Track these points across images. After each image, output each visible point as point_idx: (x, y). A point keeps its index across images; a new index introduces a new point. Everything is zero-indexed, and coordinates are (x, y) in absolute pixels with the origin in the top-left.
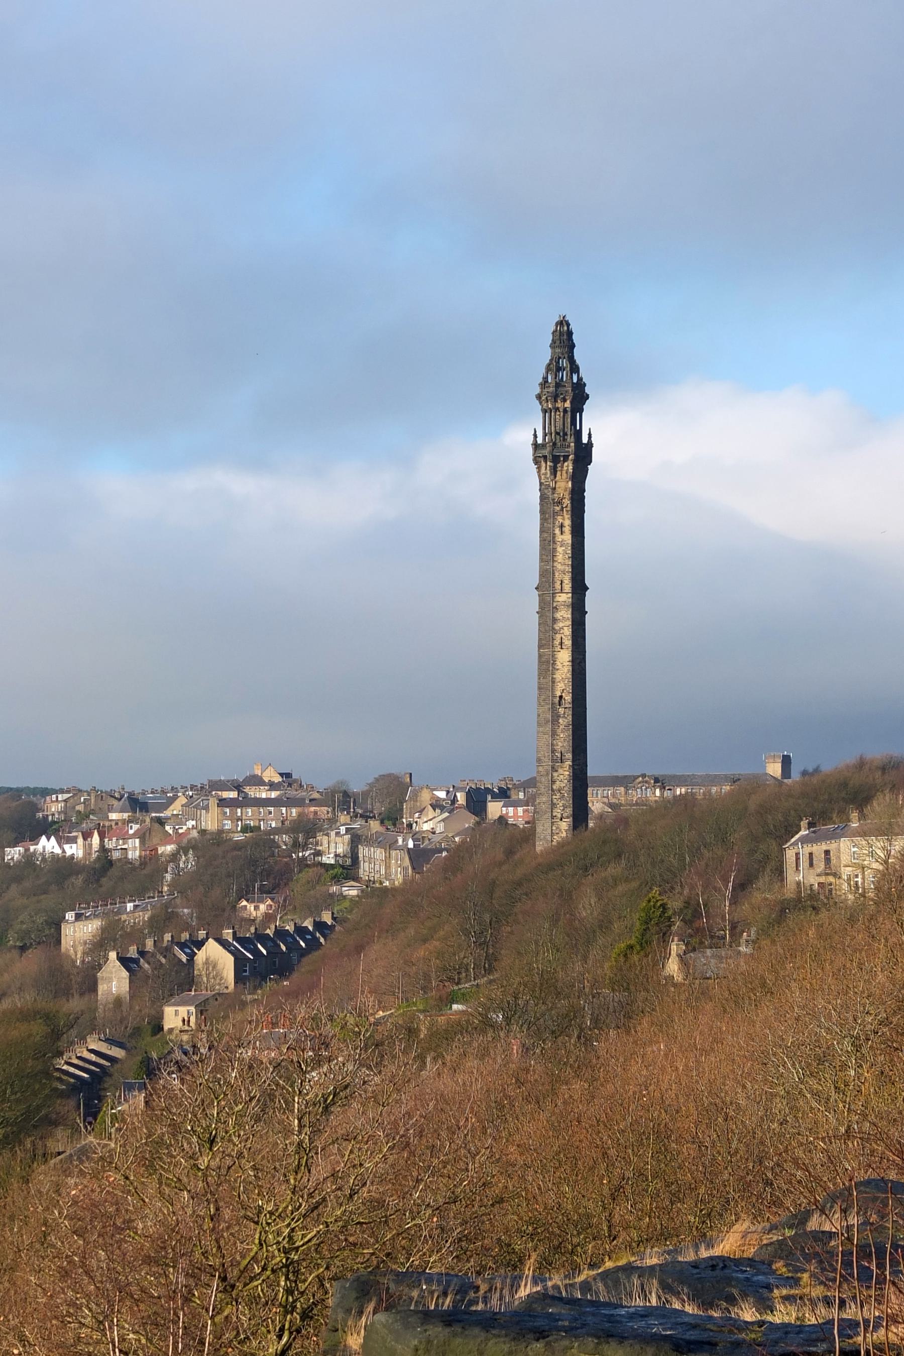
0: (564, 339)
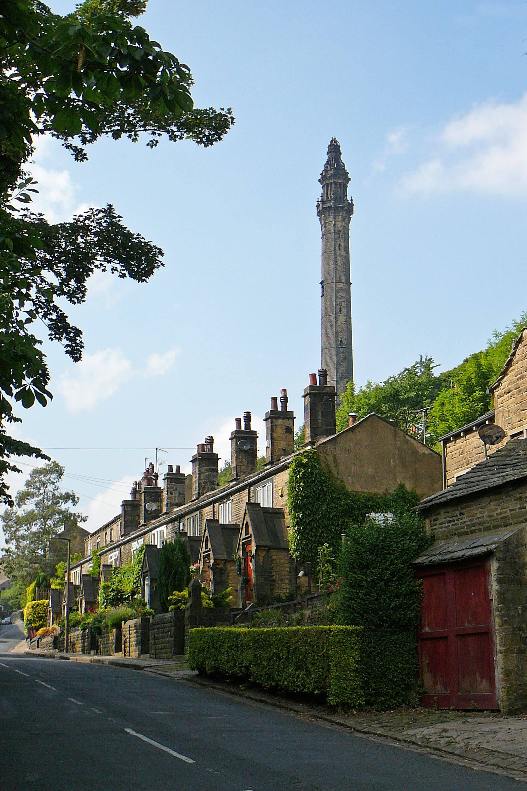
0: (334, 149)
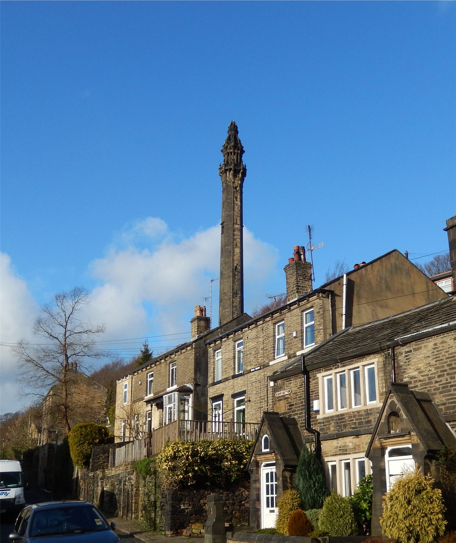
0: (234, 129)
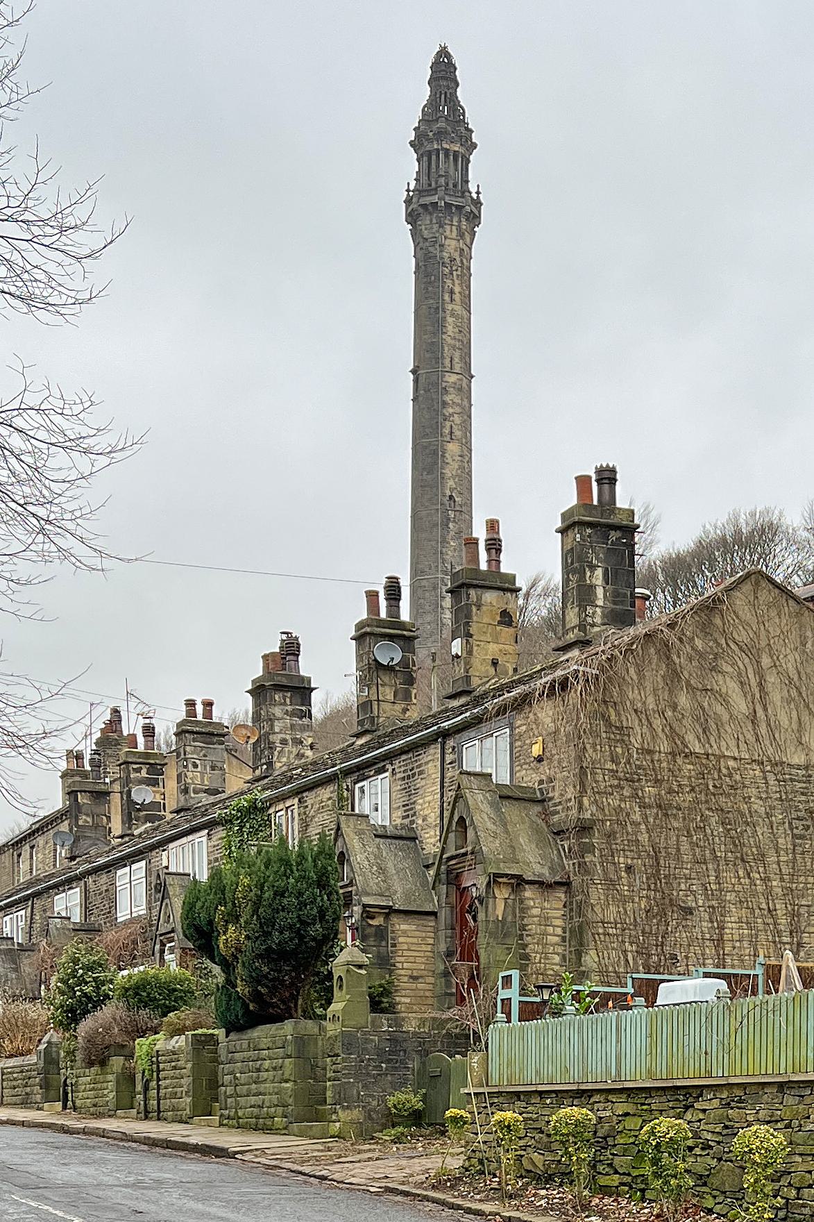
0: (443, 72)
